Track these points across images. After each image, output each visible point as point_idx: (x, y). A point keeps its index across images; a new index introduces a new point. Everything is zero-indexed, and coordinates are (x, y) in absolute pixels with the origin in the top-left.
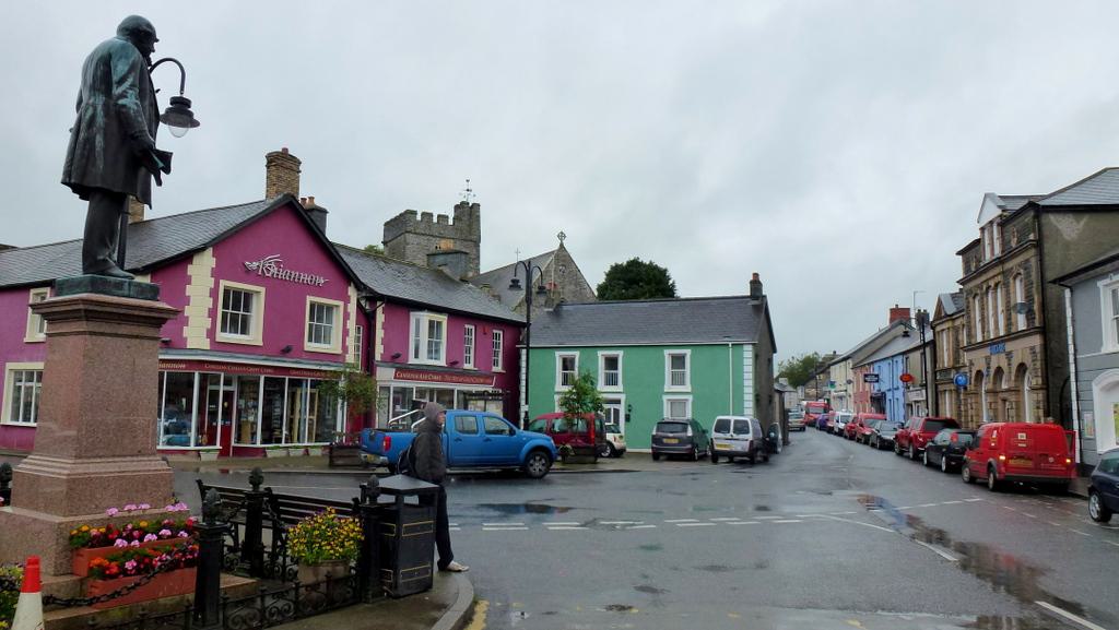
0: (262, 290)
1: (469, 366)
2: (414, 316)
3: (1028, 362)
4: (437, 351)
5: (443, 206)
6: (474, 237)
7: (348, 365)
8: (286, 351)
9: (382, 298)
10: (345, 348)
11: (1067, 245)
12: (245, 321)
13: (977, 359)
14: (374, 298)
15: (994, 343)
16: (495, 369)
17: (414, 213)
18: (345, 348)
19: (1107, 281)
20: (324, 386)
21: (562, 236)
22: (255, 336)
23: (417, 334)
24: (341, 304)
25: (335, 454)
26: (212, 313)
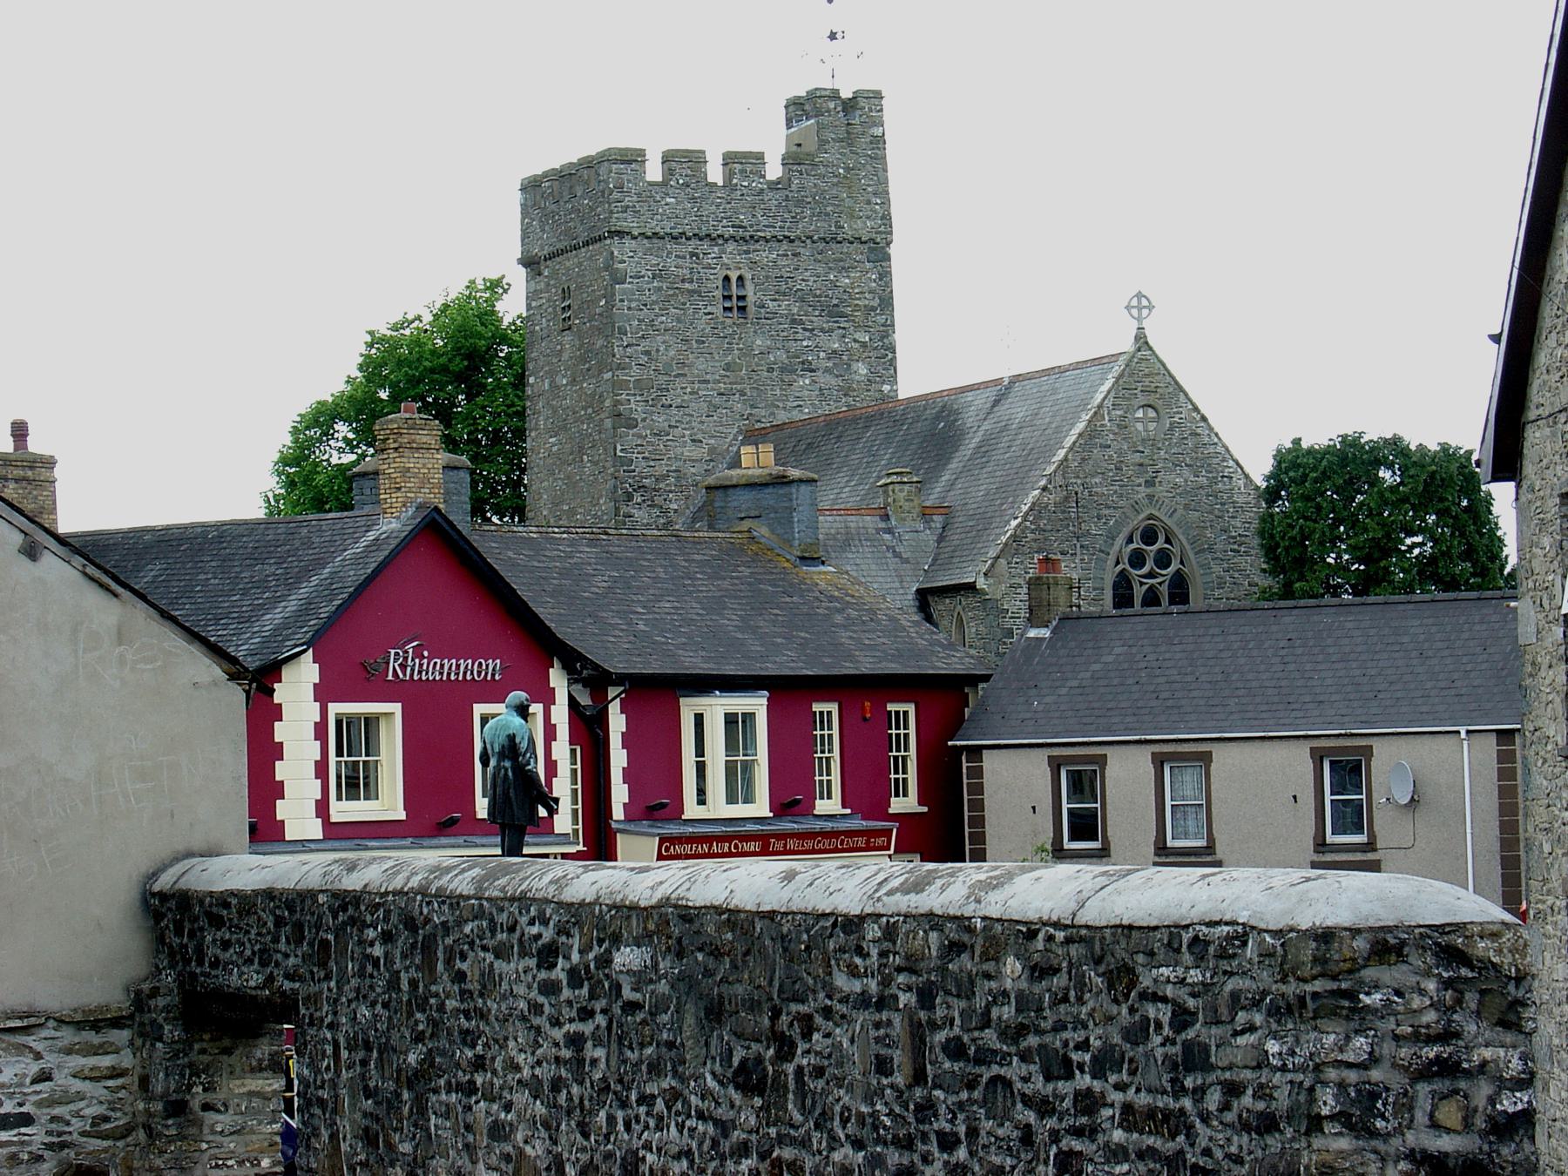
0: (396, 708)
2: (688, 708)
6: (864, 227)
9: (621, 679)
16: (898, 805)
17: (633, 158)
21: (1140, 304)
23: (700, 751)
26: (321, 769)
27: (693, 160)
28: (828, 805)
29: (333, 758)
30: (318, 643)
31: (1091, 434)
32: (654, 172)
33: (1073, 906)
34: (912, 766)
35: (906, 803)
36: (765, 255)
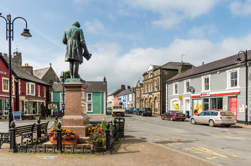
2: (27, 83)
3: (157, 97)
4: (33, 92)
9: (20, 78)
11: (166, 75)
13: (146, 96)
14: (17, 78)
15: (150, 93)
19: (175, 83)
23: (28, 88)
28: (39, 96)
33: (137, 136)
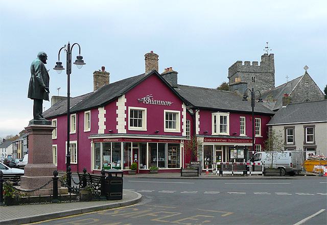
1: (243, 135)
2: (213, 115)
5: (255, 57)
6: (271, 71)
7: (184, 137)
8: (156, 133)
10: (182, 130)
12: (140, 121)
16: (257, 136)
17: (241, 62)
18: (182, 130)
20: (174, 145)
21: (306, 68)
22: (144, 127)
24: (179, 112)
25: (266, 171)
26: (126, 120)
27: (249, 62)
29: (129, 118)
30: (127, 94)
31: (298, 86)
32: (243, 64)
34: (260, 129)
35: (259, 135)
36: (258, 75)
